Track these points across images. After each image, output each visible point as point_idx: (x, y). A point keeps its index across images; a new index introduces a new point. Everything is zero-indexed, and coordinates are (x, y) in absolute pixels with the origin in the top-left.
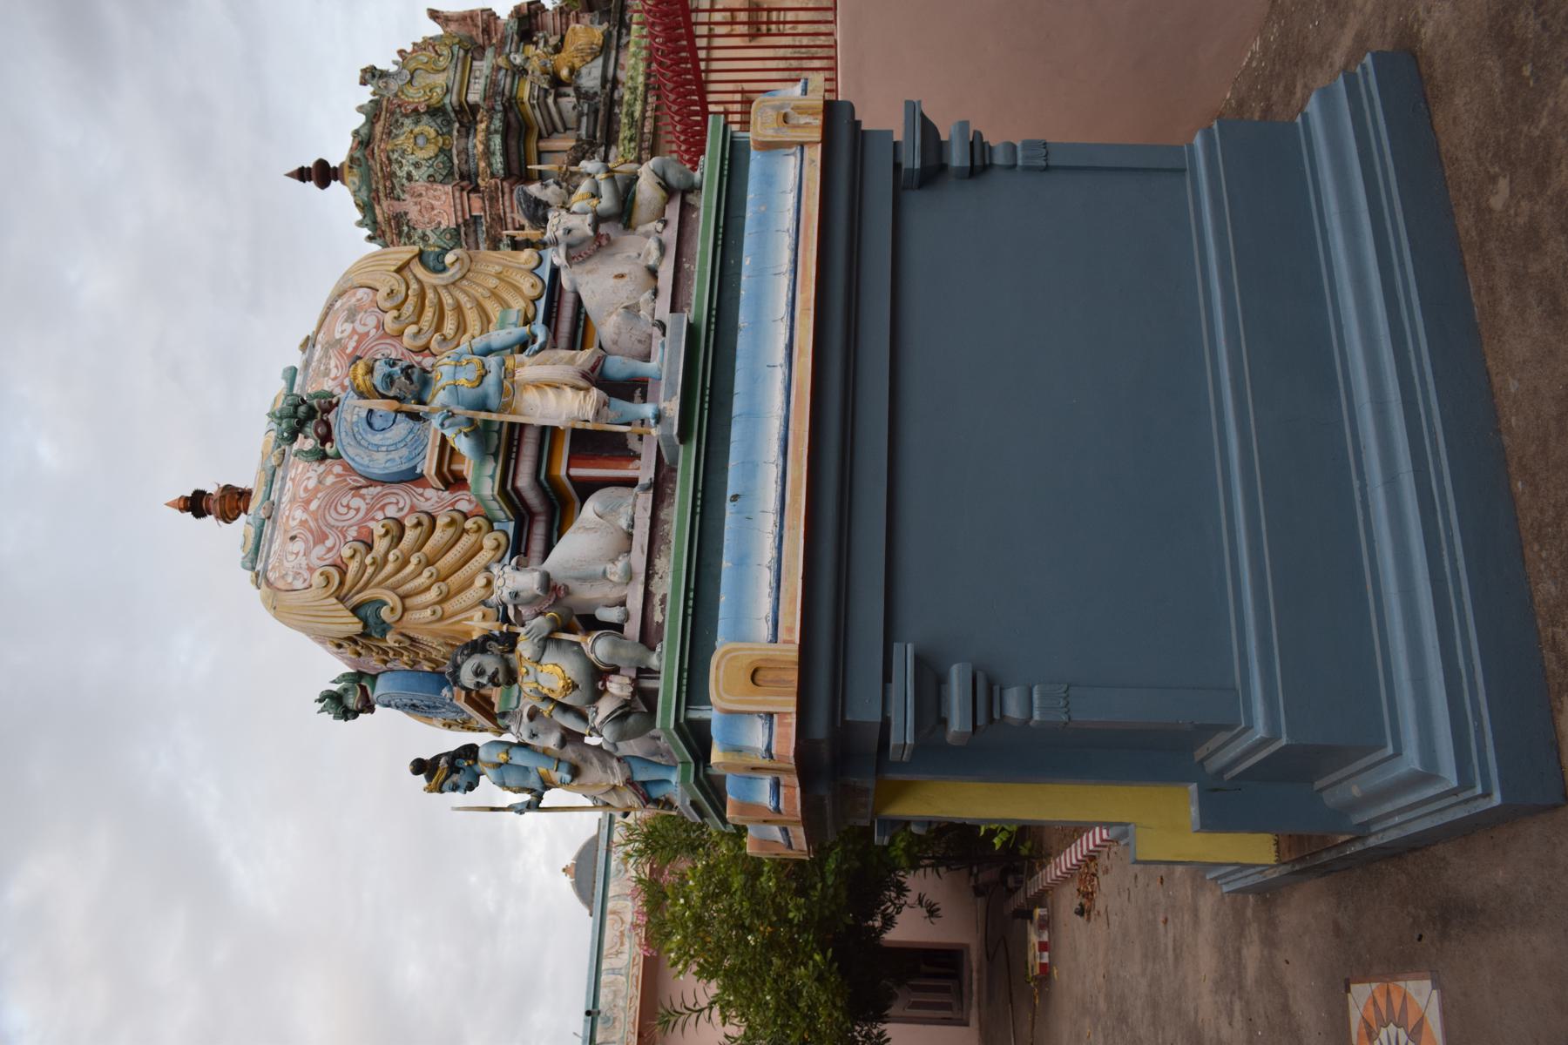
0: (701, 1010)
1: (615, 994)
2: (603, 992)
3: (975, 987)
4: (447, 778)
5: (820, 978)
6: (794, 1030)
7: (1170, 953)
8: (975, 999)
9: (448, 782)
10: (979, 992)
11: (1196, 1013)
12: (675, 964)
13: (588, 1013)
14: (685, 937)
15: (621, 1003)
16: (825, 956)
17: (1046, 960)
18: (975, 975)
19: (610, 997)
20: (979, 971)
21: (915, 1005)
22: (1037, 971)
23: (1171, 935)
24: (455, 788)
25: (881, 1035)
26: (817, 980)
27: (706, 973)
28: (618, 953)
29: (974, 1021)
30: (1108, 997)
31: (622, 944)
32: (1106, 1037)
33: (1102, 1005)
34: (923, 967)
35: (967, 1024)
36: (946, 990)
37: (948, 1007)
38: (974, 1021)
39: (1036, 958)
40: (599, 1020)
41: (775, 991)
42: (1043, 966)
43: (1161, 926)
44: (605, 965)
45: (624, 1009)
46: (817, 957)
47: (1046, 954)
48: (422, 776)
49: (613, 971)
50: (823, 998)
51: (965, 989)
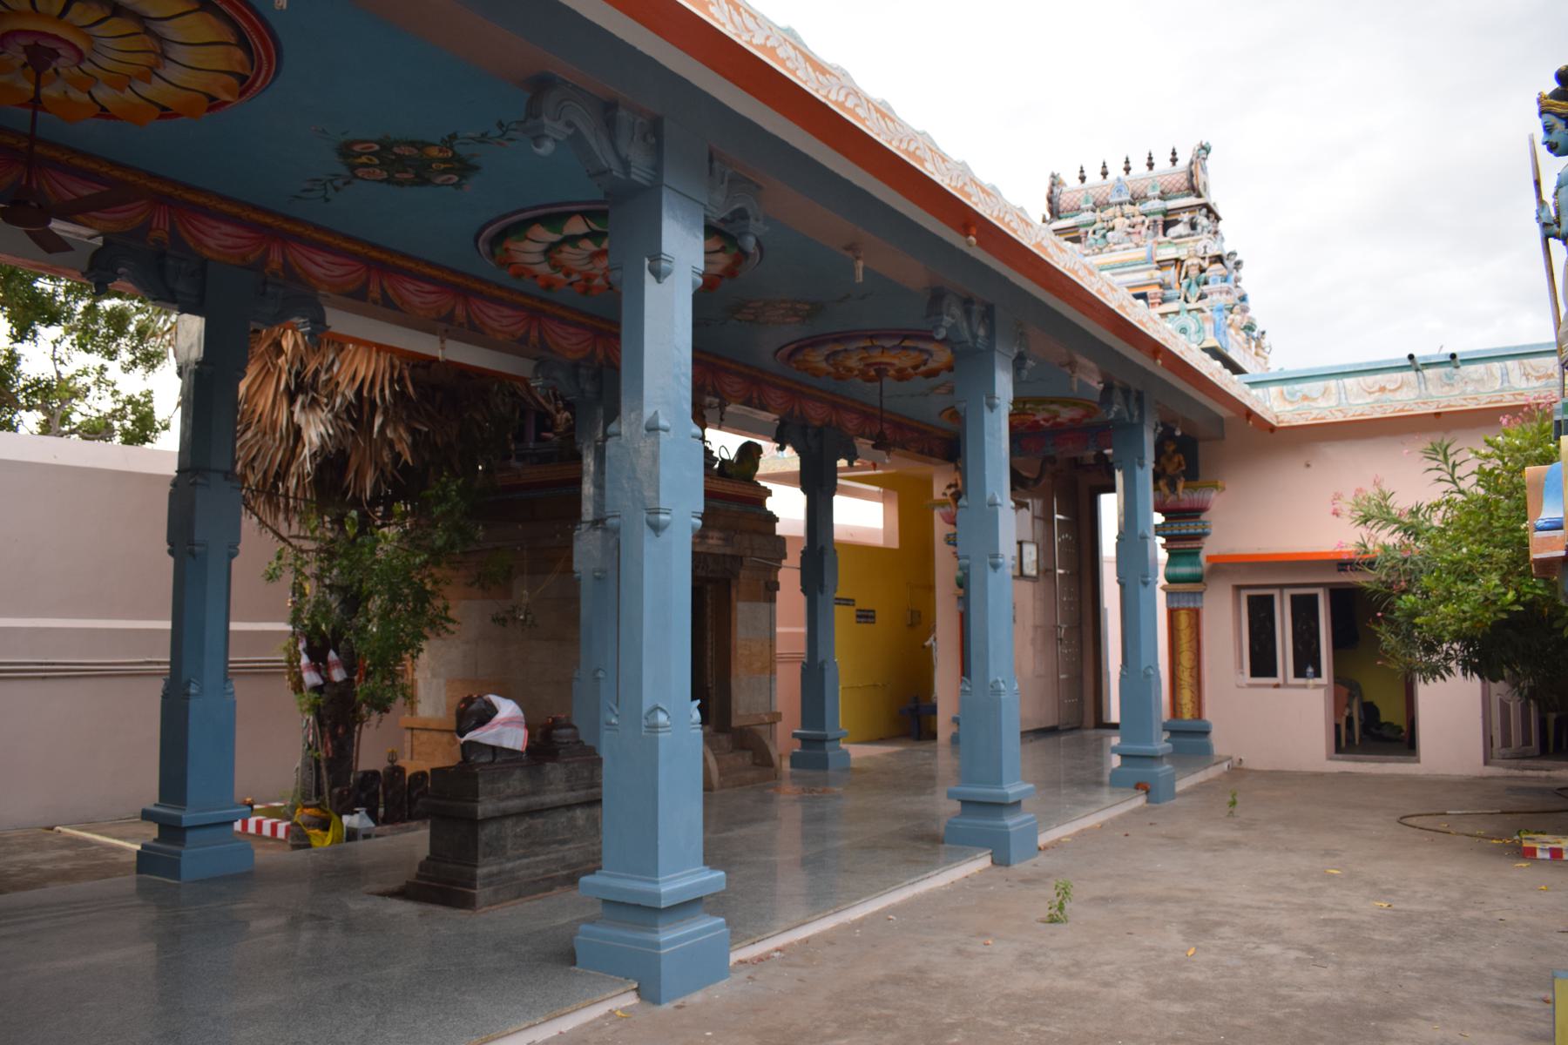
0: (1454, 482)
1: (1480, 381)
2: (1480, 368)
3: (1529, 773)
4: (1558, 115)
5: (1488, 602)
6: (1437, 579)
7: (1506, 1000)
8: (1516, 773)
9: (1552, 119)
10: (1538, 778)
11: (1427, 1019)
12: (1489, 443)
13: (1453, 356)
14: (1519, 449)
15: (1470, 389)
16: (1512, 604)
17: (1540, 855)
18: (1544, 774)
19: (1475, 376)
20: (1548, 778)
21: (1505, 708)
22: (1526, 844)
23: (1527, 1004)
24: (1548, 129)
25: (1449, 670)
26: (1487, 599)
27: (1486, 477)
28: (1527, 376)
29: (1490, 771)
30: (1477, 922)
31: (1538, 378)
32: (1431, 914)
33: (1468, 914)
34: (1552, 716)
35: (1486, 763)
36: (1527, 741)
37: (1506, 742)
38: (1490, 771)
39: (1542, 844)
40: (1448, 369)
41: (1471, 556)
42: (1532, 851)
43: (1542, 994)
44: (1510, 363)
45: (1463, 392)
46: (1511, 595)
47: (1547, 856)
48: (1556, 85)
49: (1505, 374)
50: (1465, 607)
51: (1527, 762)
